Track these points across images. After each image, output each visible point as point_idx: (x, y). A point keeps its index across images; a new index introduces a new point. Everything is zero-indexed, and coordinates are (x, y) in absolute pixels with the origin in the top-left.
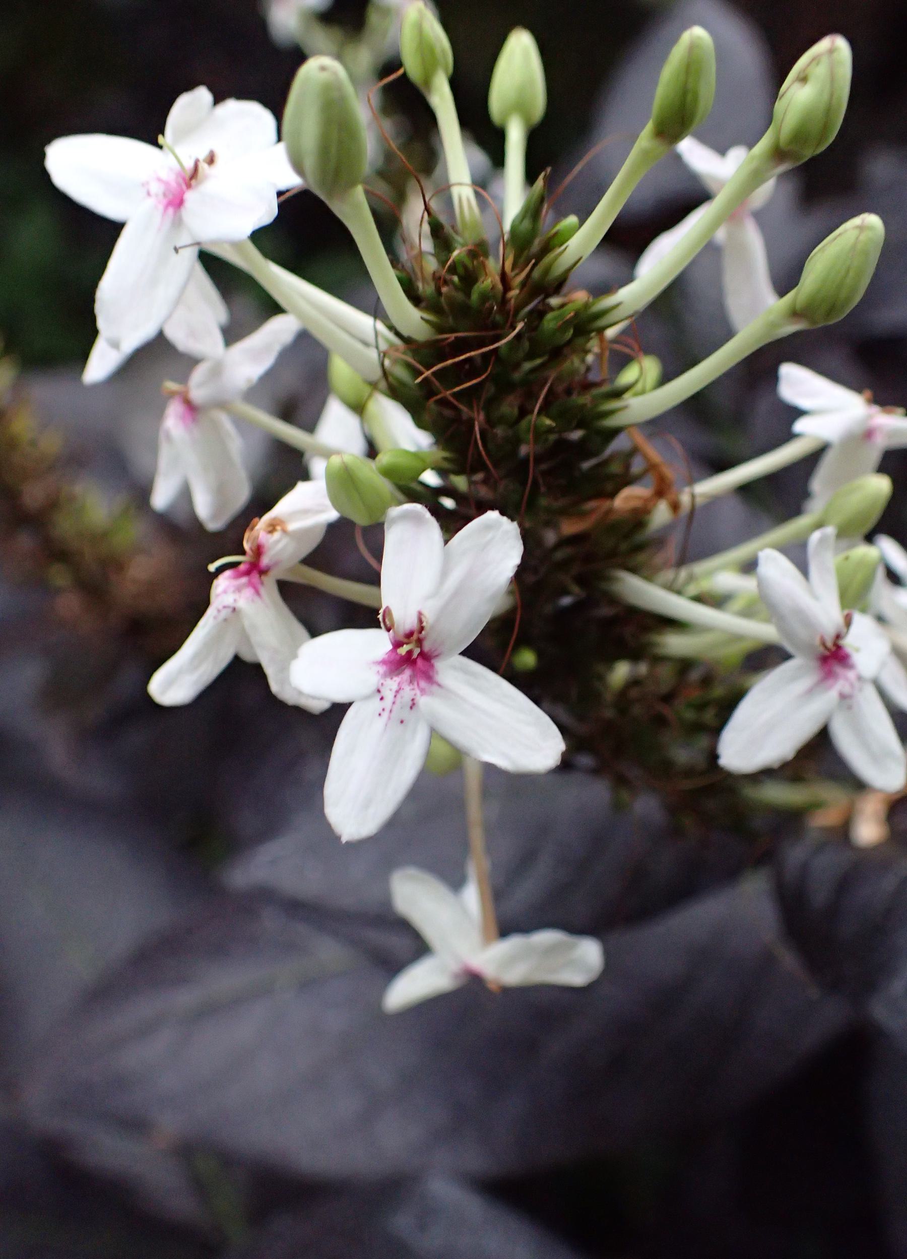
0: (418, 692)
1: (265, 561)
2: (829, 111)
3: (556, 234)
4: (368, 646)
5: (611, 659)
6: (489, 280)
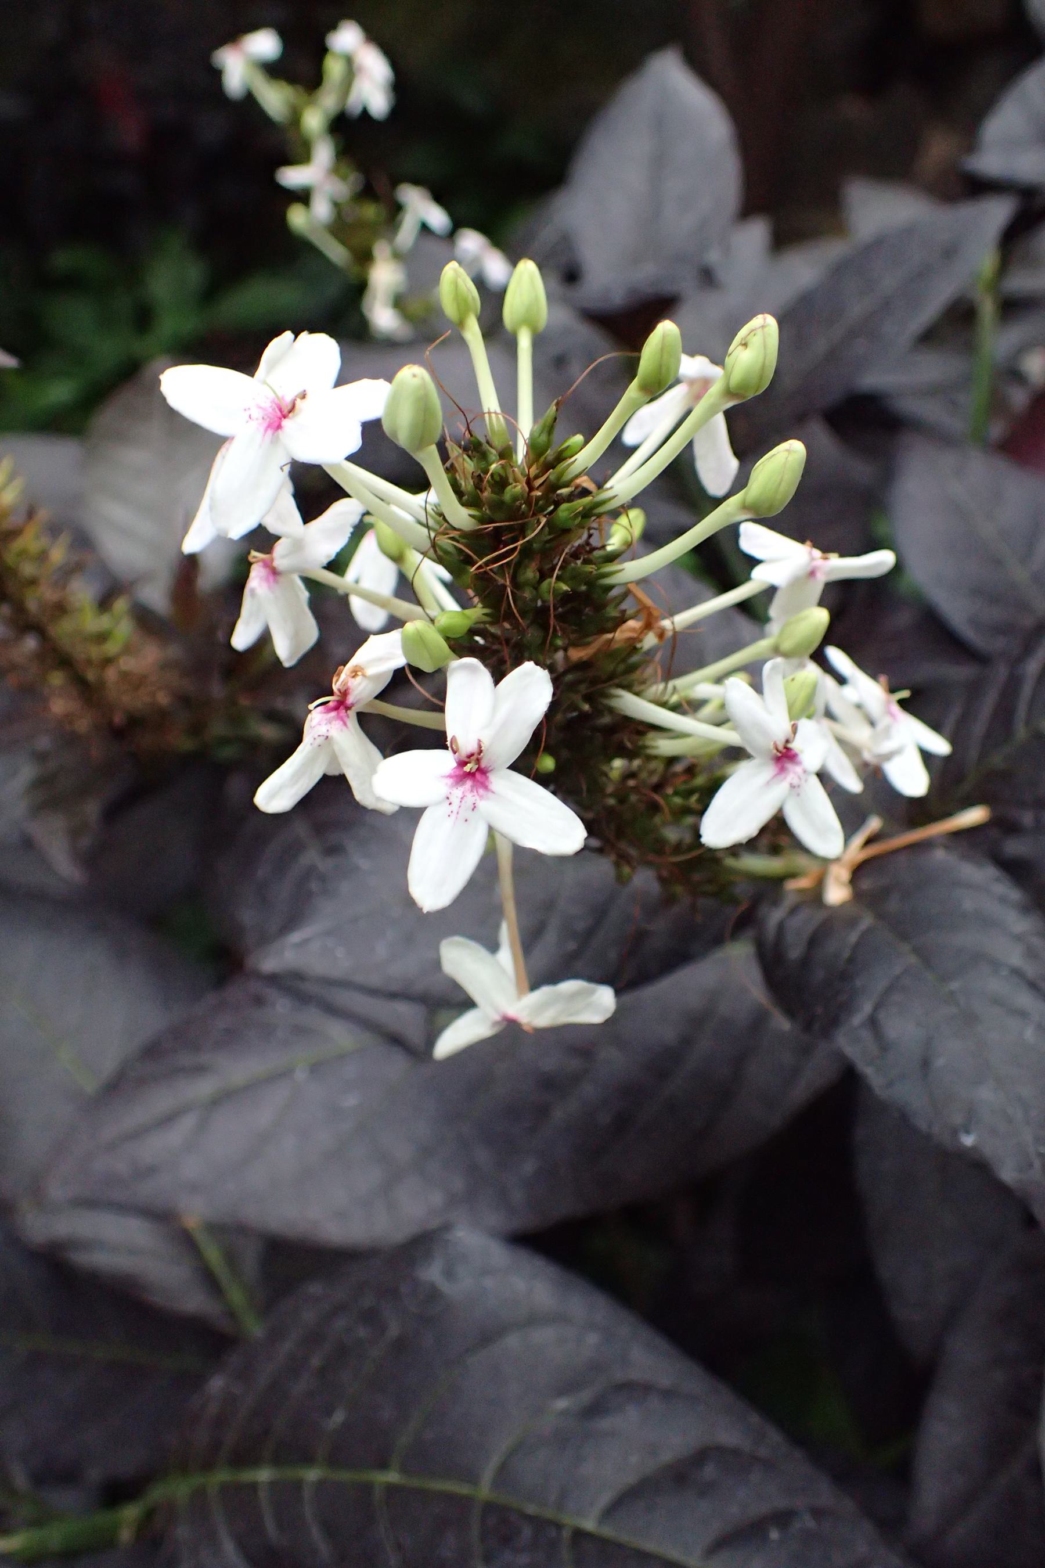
0: (477, 798)
1: (350, 699)
2: (763, 367)
3: (568, 447)
4: (433, 764)
5: (610, 759)
6: (517, 488)
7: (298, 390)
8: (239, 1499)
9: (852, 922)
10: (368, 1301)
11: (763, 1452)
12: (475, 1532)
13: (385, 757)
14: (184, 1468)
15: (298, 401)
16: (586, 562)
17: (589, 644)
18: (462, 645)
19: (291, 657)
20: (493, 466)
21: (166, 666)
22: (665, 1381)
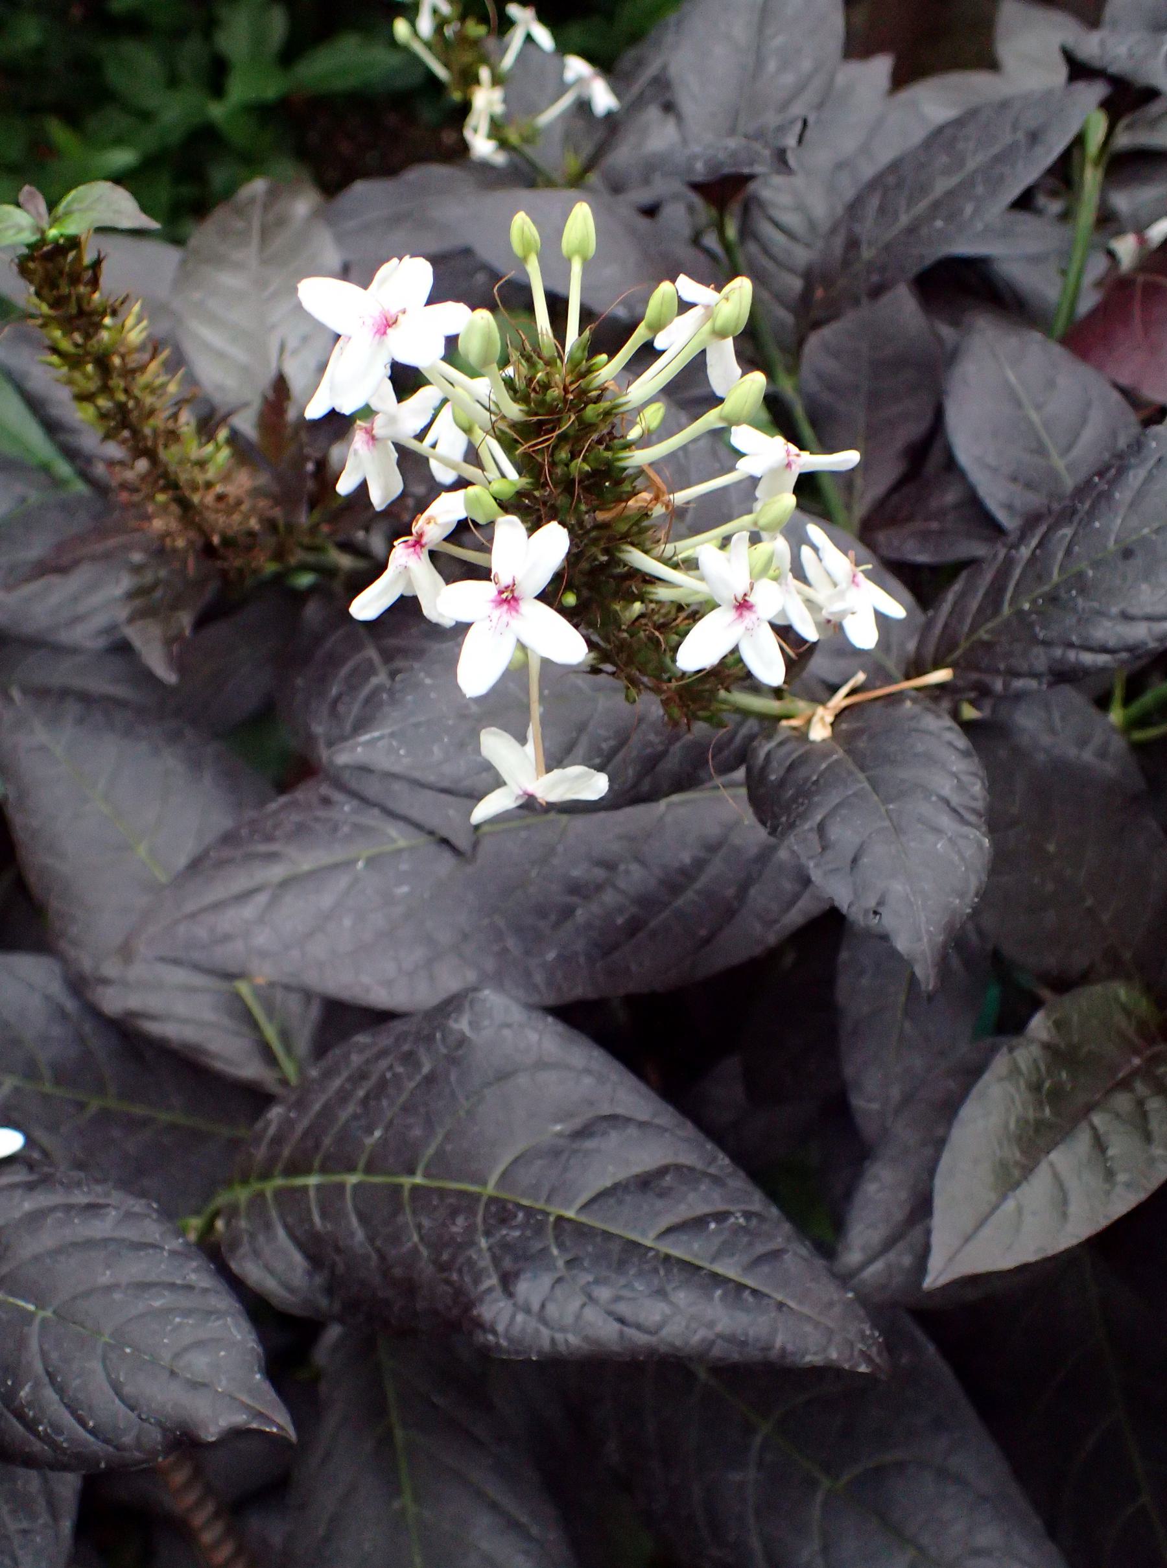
1: (425, 540)
2: (738, 318)
6: (555, 393)
7: (400, 308)
8: (291, 1199)
9: (826, 755)
10: (406, 1047)
11: (712, 1170)
12: (479, 1219)
13: (447, 583)
14: (245, 1181)
15: (400, 315)
16: (608, 448)
17: (609, 509)
18: (506, 506)
19: (380, 505)
20: (539, 375)
21: (256, 492)
22: (643, 1116)
